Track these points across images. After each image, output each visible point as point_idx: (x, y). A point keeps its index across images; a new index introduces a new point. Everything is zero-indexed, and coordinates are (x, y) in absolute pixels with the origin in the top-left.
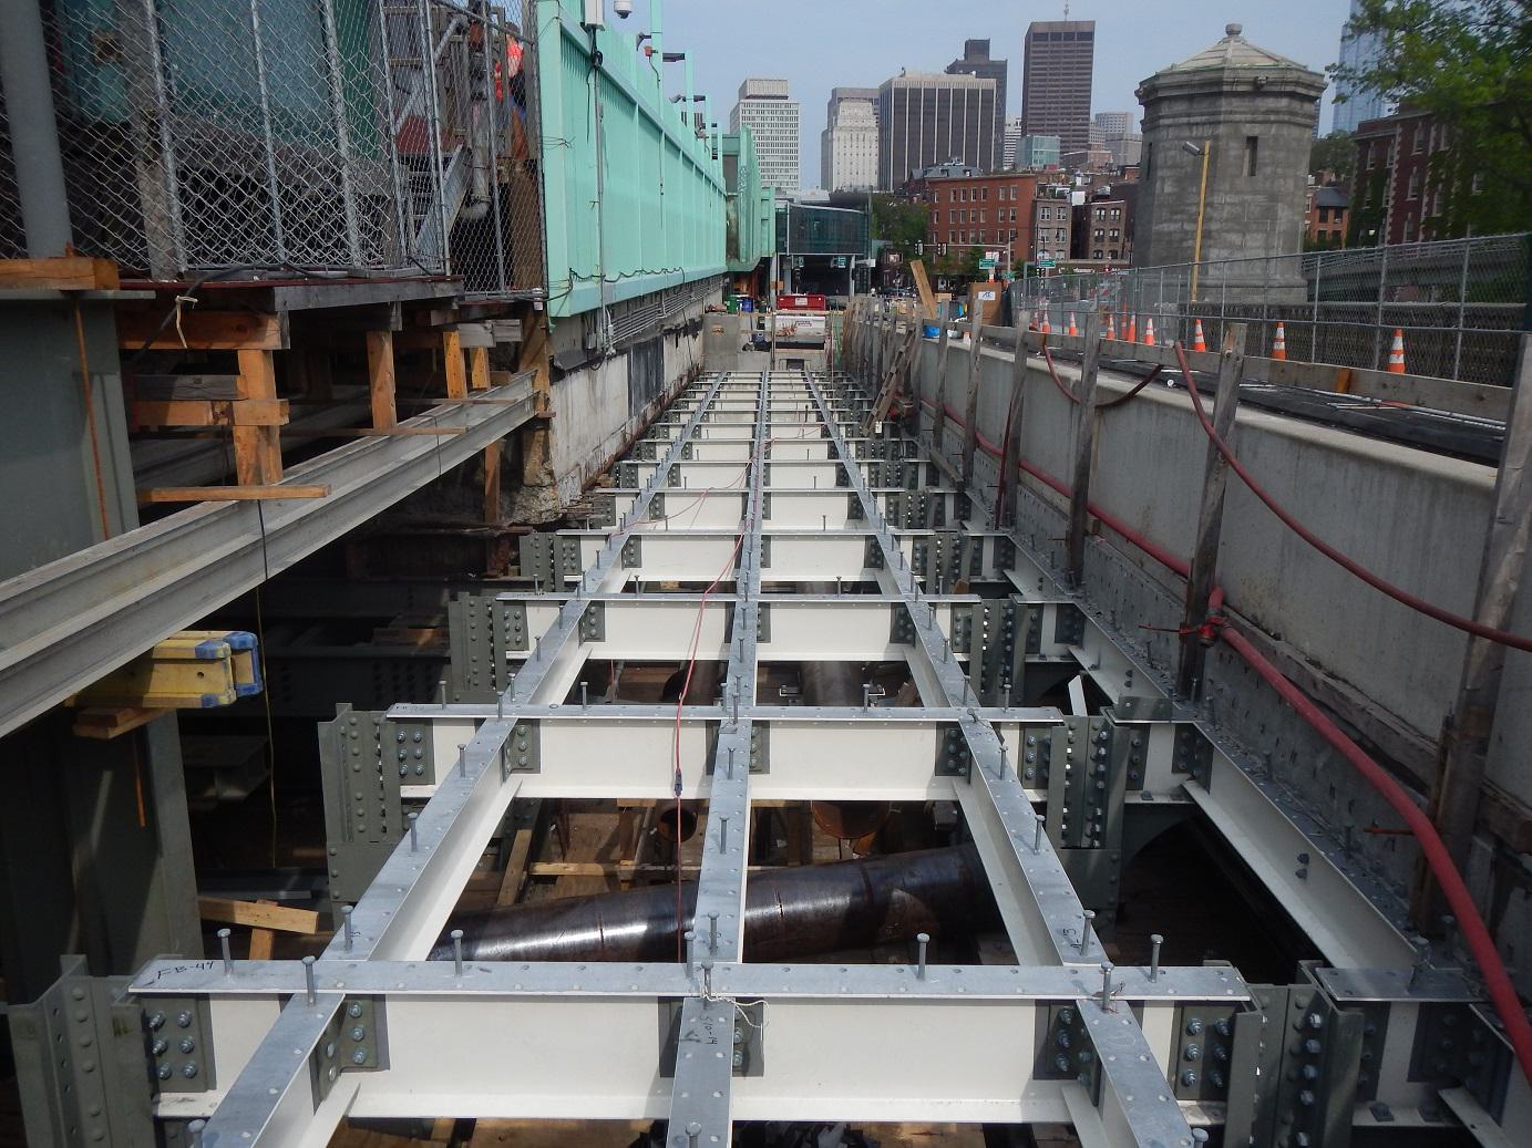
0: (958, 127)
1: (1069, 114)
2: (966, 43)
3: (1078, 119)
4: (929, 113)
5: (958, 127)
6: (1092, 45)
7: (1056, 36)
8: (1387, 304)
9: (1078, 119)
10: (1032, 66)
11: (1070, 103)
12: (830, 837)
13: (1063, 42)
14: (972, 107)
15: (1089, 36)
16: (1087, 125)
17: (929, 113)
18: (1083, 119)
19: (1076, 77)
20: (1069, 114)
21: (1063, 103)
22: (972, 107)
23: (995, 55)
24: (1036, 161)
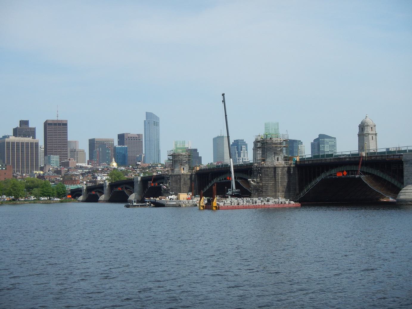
0: (27, 153)
1: (61, 148)
2: (20, 121)
3: (64, 150)
4: (18, 149)
5: (27, 153)
6: (67, 127)
7: (55, 124)
8: (386, 153)
9: (64, 150)
10: (394, 148)
11: (61, 145)
12: (407, 159)
13: (53, 126)
14: (32, 148)
15: (66, 124)
16: (67, 151)
17: (18, 149)
18: (65, 150)
19: (58, 137)
20: (61, 148)
21: (59, 144)
22: (32, 148)
23: (31, 126)
24: (52, 163)
